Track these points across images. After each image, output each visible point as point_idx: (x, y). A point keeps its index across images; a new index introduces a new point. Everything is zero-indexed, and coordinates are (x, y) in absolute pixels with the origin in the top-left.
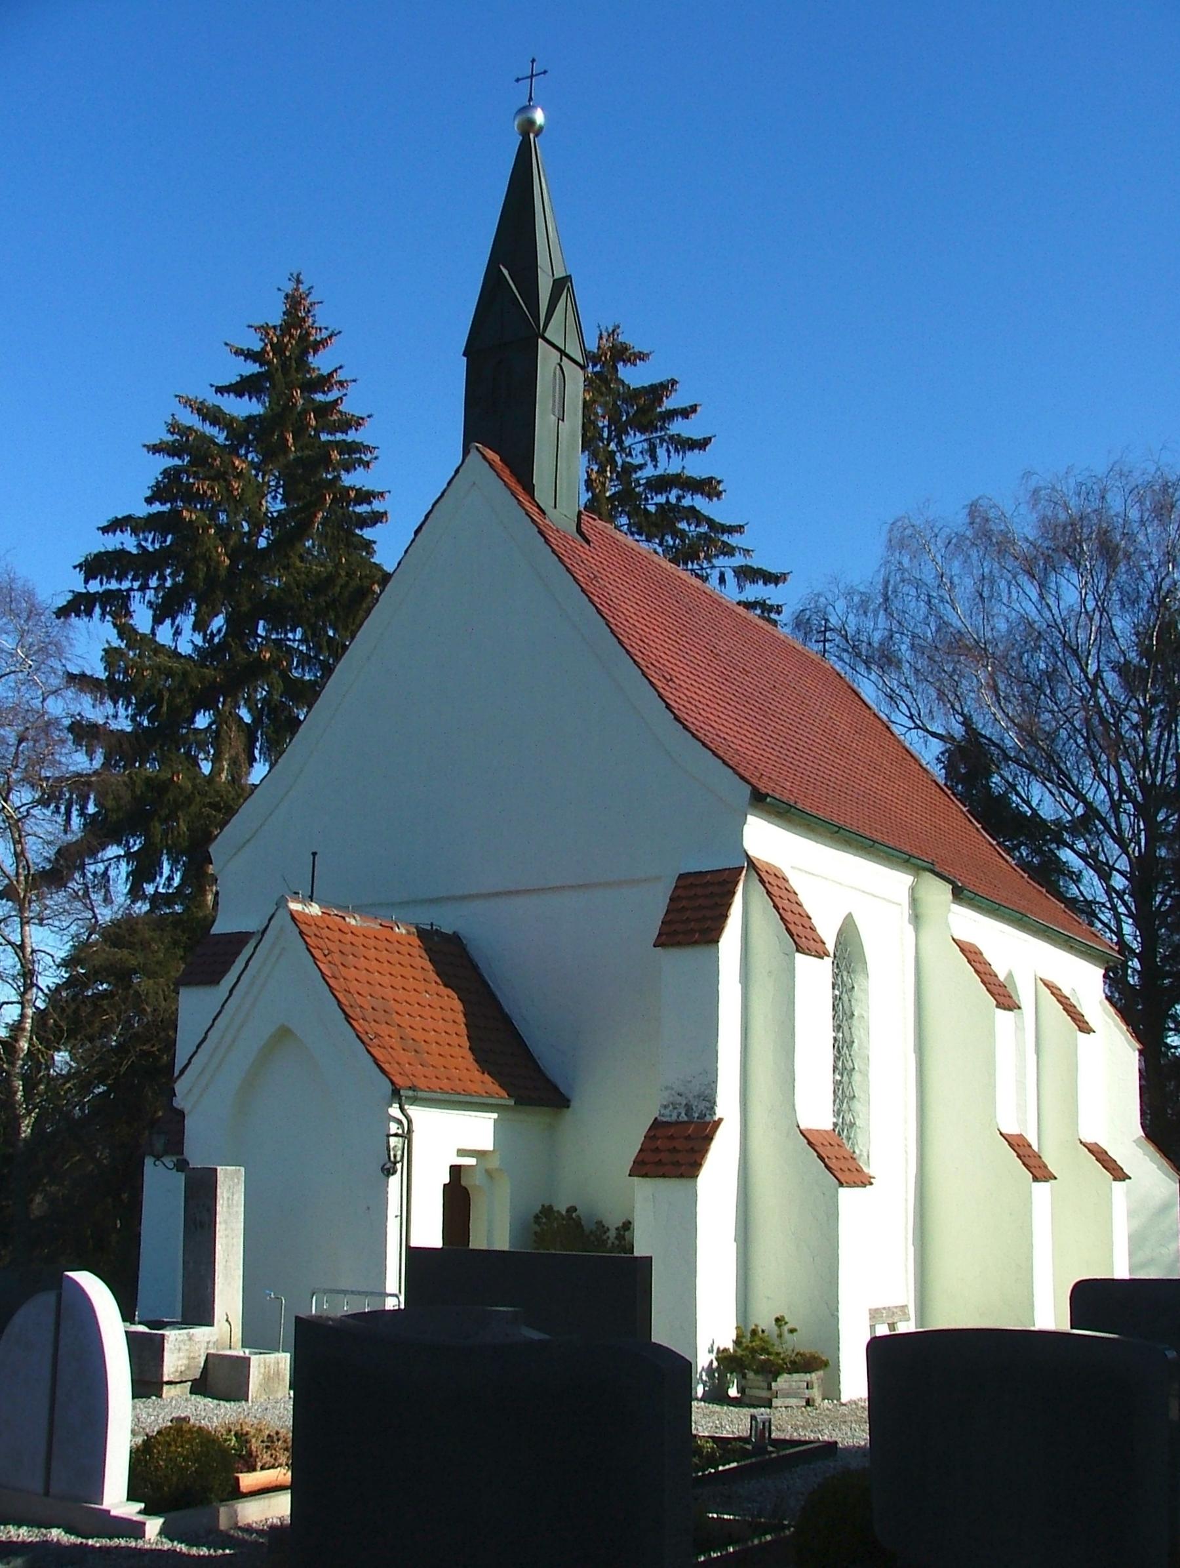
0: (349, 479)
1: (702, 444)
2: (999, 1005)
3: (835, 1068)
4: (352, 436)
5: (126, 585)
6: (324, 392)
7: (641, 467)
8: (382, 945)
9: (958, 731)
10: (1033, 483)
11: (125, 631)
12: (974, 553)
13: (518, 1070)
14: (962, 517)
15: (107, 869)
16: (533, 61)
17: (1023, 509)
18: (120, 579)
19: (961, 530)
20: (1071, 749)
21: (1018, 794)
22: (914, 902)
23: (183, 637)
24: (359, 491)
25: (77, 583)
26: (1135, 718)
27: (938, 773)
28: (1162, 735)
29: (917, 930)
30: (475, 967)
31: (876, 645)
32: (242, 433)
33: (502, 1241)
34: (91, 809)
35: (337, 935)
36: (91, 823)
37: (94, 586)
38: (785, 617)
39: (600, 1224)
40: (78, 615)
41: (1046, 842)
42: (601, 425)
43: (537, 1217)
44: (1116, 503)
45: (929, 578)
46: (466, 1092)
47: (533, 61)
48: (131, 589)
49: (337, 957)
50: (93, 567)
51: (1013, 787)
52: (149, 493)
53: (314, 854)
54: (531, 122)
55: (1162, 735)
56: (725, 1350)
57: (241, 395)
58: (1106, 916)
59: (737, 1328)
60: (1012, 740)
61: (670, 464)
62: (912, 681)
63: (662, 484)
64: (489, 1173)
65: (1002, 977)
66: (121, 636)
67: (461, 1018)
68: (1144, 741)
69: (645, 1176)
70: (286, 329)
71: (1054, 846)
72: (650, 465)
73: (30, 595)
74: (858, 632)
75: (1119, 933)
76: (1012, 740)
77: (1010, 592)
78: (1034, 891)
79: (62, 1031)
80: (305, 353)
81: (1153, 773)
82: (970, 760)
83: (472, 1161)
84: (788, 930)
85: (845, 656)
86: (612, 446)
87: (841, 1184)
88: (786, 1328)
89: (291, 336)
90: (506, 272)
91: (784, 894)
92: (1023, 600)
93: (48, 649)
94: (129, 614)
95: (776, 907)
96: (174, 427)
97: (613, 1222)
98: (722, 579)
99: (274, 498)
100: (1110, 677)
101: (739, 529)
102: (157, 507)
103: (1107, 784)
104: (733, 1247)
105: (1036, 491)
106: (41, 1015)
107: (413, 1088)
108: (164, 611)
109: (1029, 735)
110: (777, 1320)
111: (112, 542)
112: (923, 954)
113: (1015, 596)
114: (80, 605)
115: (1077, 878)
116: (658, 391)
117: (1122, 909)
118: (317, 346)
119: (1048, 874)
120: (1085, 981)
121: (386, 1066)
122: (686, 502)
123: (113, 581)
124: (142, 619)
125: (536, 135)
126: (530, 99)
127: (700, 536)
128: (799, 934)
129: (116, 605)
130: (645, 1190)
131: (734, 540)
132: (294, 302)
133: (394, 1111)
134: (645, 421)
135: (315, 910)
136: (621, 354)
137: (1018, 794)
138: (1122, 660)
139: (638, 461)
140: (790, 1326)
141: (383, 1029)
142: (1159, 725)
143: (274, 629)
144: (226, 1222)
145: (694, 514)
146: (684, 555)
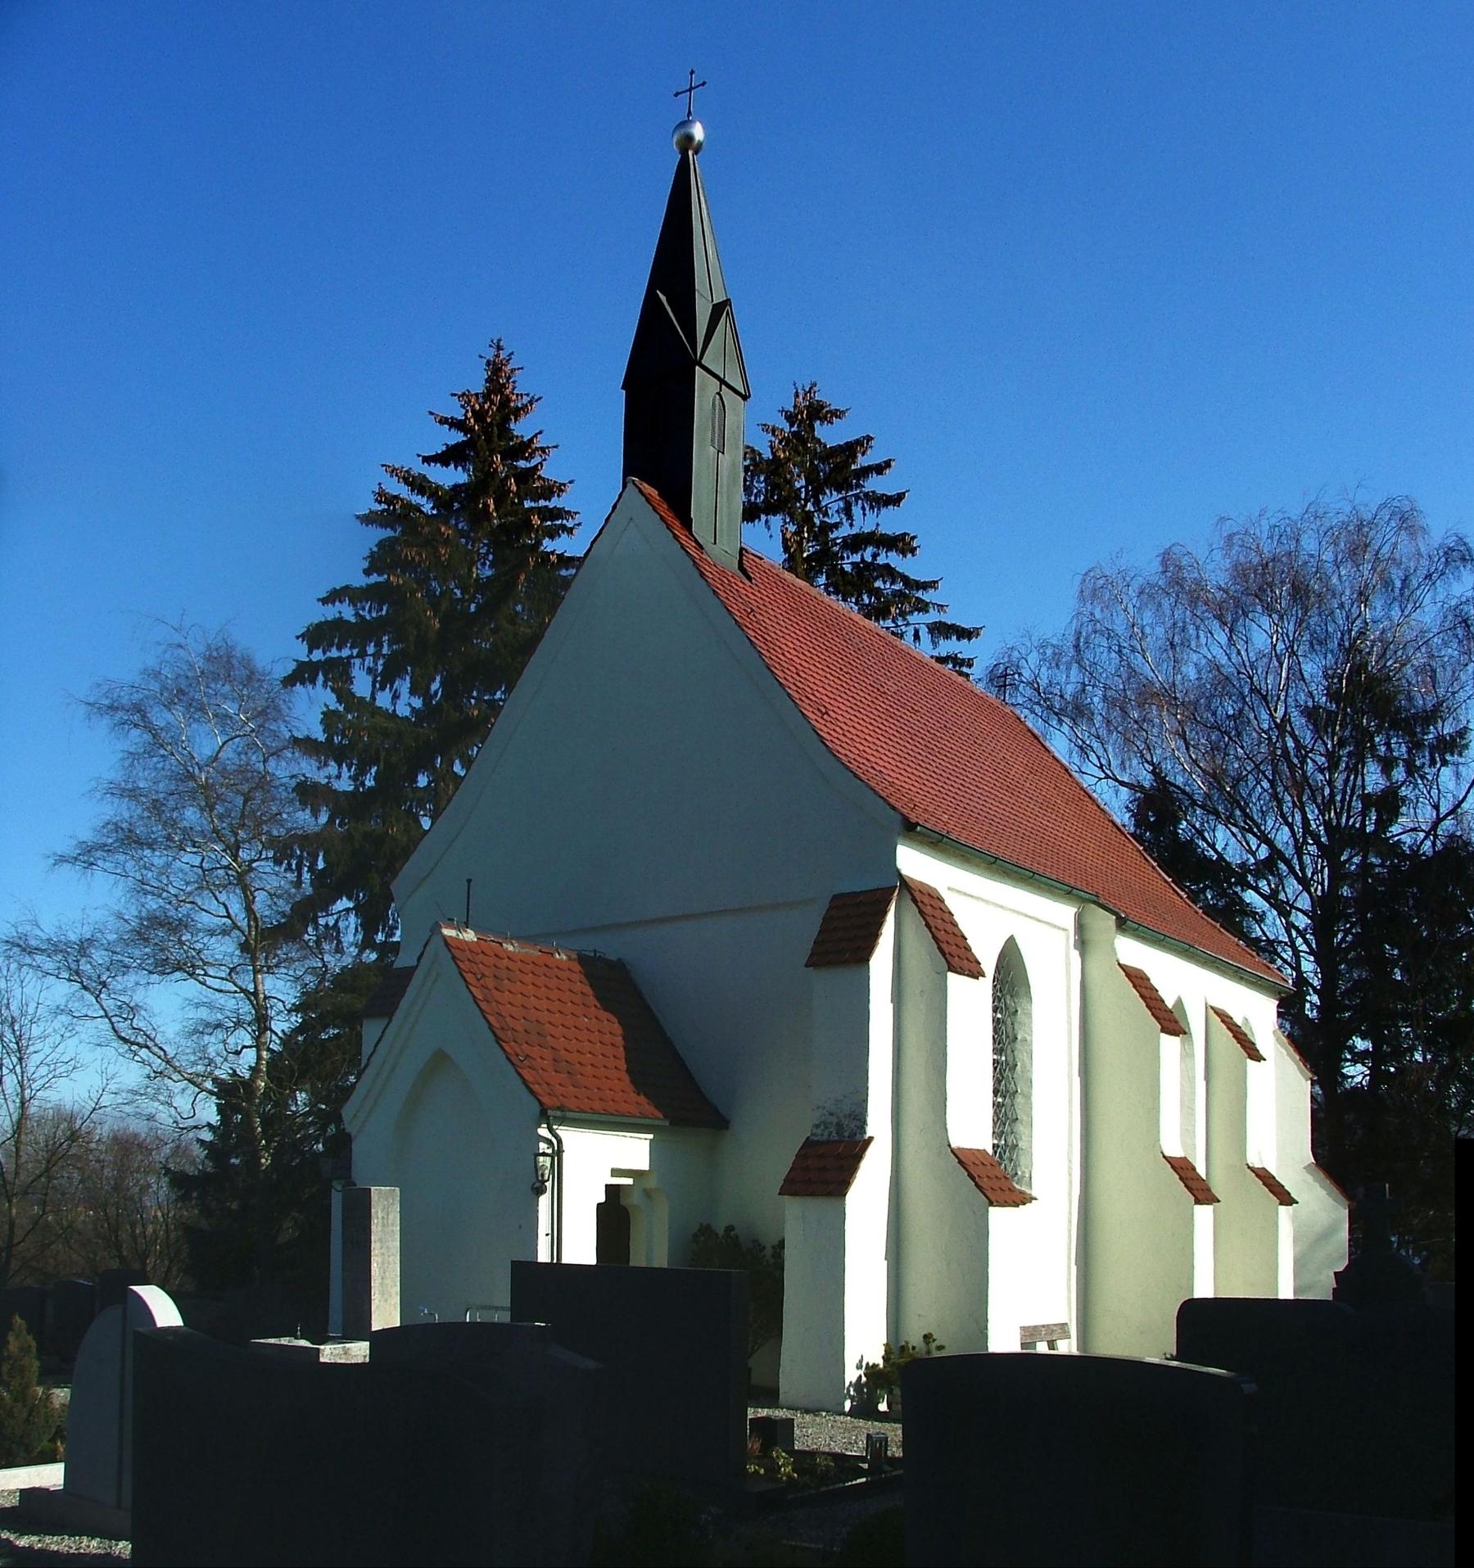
0: (548, 545)
1: (896, 500)
2: (1165, 1030)
3: (996, 1092)
4: (554, 502)
5: (345, 653)
6: (526, 459)
7: (836, 526)
8: (541, 971)
9: (1147, 779)
10: (1228, 528)
11: (344, 694)
12: (1166, 604)
13: (672, 1089)
14: (1156, 566)
15: (337, 921)
16: (692, 72)
17: (1217, 555)
18: (339, 649)
19: (1154, 579)
20: (1258, 792)
21: (1204, 839)
22: (1080, 927)
23: (403, 702)
24: (560, 557)
25: (301, 651)
26: (1321, 760)
27: (1123, 818)
28: (1348, 777)
29: (1083, 955)
30: (639, 994)
31: (1067, 697)
32: (445, 500)
33: (660, 1259)
34: (321, 865)
35: (492, 960)
36: (319, 878)
37: (318, 655)
38: (977, 671)
39: (756, 1241)
40: (303, 683)
41: (1230, 885)
42: (797, 485)
43: (695, 1236)
44: (1309, 544)
45: (1120, 627)
46: (594, 1111)
47: (692, 72)
48: (351, 657)
49: (490, 982)
50: (316, 636)
51: (1200, 833)
52: (366, 565)
53: (469, 881)
54: (689, 138)
55: (1348, 777)
56: (875, 1366)
57: (447, 465)
58: (1288, 955)
59: (887, 1345)
60: (1199, 786)
61: (865, 521)
62: (1103, 732)
63: (856, 543)
64: (647, 1193)
65: (1170, 1003)
66: (339, 701)
67: (619, 1040)
68: (1330, 783)
69: (794, 1194)
70: (487, 396)
71: (1238, 889)
72: (846, 524)
73: (247, 662)
74: (1050, 684)
75: (1297, 967)
76: (1199, 786)
77: (1198, 637)
78: (1211, 928)
79: (293, 1071)
80: (507, 420)
81: (1339, 816)
82: (1158, 807)
83: (629, 1181)
84: (940, 948)
85: (1037, 709)
86: (810, 507)
87: (991, 1204)
88: (933, 1345)
89: (492, 403)
90: (663, 298)
91: (937, 913)
92: (1213, 644)
93: (267, 713)
94: (350, 680)
95: (928, 925)
96: (382, 496)
97: (770, 1241)
98: (917, 636)
99: (484, 564)
100: (1298, 721)
101: (933, 585)
102: (375, 578)
103: (1291, 826)
104: (883, 1266)
105: (1230, 537)
106: (276, 1057)
107: (561, 1108)
108: (385, 679)
109: (1215, 778)
110: (925, 1337)
111: (330, 612)
112: (1089, 979)
113: (1203, 640)
114: (303, 674)
115: (1261, 919)
116: (851, 449)
117: (1304, 948)
118: (517, 412)
119: (1232, 916)
120: (1258, 1012)
121: (536, 1087)
122: (881, 560)
123: (334, 649)
124: (362, 685)
125: (696, 152)
126: (689, 113)
127: (895, 593)
128: (955, 955)
129: (338, 673)
130: (793, 1208)
131: (926, 596)
132: (496, 369)
133: (543, 1131)
134: (840, 479)
135: (470, 936)
136: (818, 412)
137: (1204, 839)
138: (1310, 704)
139: (835, 519)
140: (937, 1343)
141: (535, 1051)
142: (1347, 766)
143: (485, 692)
144: (380, 1240)
145: (889, 572)
146: (878, 612)
